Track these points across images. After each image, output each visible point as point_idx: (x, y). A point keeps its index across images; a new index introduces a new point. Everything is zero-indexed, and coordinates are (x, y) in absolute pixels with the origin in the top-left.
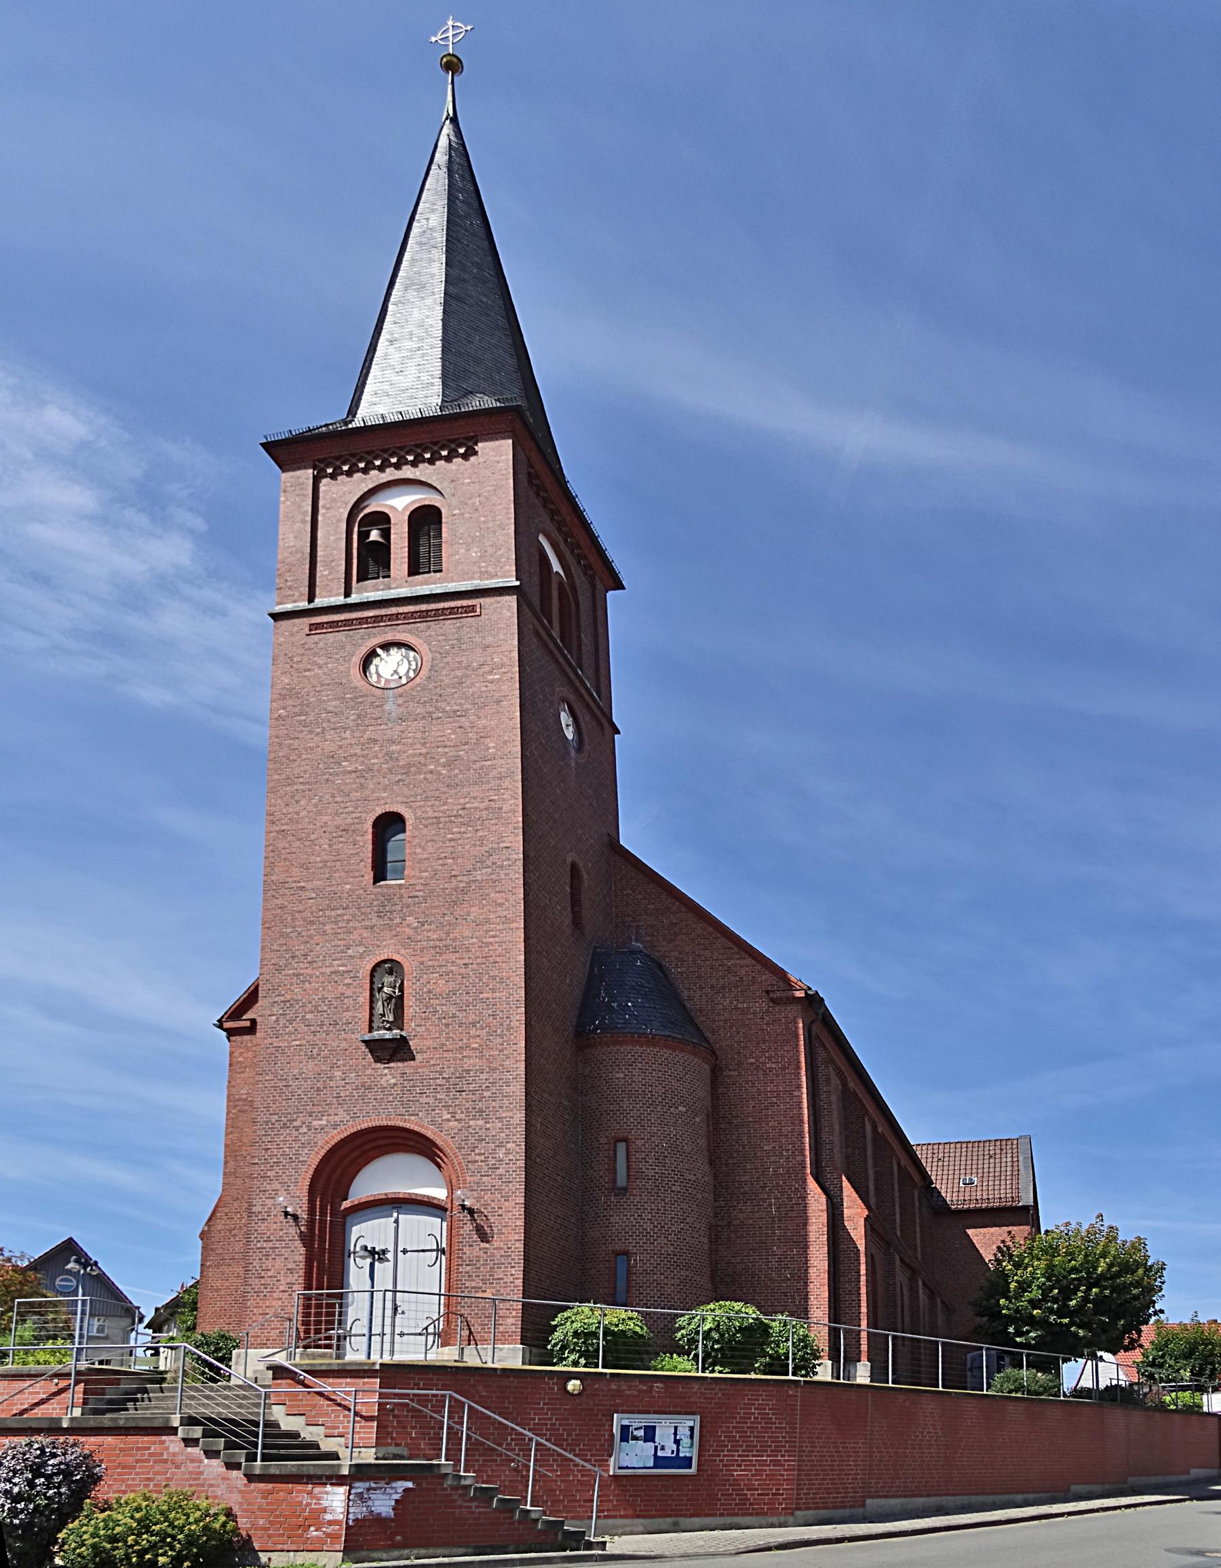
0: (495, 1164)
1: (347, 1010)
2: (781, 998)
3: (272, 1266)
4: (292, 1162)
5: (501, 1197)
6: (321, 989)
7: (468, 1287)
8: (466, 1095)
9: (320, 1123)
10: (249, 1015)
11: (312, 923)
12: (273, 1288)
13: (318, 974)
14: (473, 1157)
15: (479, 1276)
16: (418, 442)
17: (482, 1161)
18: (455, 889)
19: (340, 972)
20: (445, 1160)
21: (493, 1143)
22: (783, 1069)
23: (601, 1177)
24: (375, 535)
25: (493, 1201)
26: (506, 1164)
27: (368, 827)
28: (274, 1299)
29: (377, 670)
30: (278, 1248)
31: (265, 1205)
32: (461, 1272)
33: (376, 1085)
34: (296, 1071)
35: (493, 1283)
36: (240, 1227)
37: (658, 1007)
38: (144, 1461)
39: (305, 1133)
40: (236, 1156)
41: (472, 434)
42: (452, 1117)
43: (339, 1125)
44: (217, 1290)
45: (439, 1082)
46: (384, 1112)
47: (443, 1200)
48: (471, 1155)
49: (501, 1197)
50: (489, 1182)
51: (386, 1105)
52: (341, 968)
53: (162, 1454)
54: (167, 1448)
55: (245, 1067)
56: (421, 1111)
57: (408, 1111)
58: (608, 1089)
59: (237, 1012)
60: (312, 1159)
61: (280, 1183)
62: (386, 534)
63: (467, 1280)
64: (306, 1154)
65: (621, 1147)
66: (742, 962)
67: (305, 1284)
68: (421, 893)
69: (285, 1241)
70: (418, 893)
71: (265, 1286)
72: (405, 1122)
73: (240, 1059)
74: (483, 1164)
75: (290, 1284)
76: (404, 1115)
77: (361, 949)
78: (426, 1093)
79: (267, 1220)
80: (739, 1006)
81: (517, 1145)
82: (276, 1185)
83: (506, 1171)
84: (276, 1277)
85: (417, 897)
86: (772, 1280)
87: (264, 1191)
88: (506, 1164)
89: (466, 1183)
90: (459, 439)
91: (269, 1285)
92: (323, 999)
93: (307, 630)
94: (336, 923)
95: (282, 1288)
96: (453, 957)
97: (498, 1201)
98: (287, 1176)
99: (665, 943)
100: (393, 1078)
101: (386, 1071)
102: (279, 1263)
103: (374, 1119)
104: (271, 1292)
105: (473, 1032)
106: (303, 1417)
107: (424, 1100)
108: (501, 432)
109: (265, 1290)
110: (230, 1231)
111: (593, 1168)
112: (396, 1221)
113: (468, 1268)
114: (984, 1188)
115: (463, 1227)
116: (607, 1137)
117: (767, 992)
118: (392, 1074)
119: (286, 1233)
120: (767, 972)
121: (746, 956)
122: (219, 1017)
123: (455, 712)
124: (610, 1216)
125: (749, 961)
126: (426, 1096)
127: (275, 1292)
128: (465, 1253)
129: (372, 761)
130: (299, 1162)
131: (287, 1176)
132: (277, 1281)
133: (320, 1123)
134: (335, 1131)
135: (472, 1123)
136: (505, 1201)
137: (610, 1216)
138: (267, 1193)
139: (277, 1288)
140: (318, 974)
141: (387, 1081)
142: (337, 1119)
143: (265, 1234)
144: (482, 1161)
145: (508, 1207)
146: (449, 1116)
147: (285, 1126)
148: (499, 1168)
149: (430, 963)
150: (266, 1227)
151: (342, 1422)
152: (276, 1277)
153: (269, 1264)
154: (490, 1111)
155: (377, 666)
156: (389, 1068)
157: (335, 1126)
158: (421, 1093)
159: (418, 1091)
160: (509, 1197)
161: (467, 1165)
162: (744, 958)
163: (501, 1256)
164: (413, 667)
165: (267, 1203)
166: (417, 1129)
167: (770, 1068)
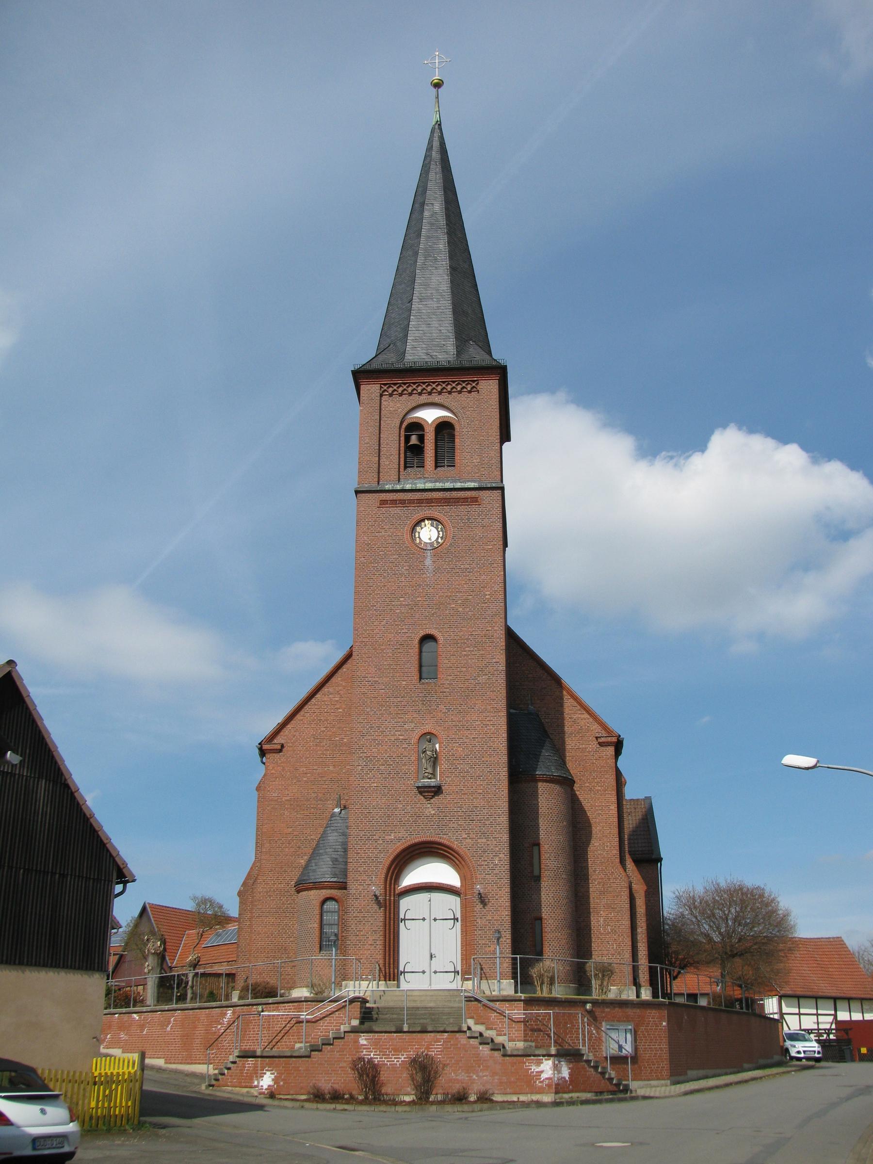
1: (405, 765)
6: (388, 750)
7: (480, 944)
9: (390, 837)
11: (382, 706)
15: (486, 937)
17: (486, 865)
18: (468, 688)
20: (463, 863)
24: (414, 440)
27: (416, 641)
29: (419, 535)
30: (366, 917)
31: (358, 889)
37: (552, 755)
38: (448, 1048)
52: (401, 737)
53: (457, 1045)
54: (460, 1041)
62: (421, 438)
66: (583, 716)
68: (448, 690)
70: (445, 690)
79: (359, 898)
81: (505, 856)
82: (364, 877)
84: (366, 935)
85: (445, 692)
86: (600, 933)
92: (390, 757)
94: (397, 706)
95: (370, 943)
96: (467, 733)
99: (539, 701)
101: (429, 806)
106: (484, 1025)
107: (451, 825)
113: (480, 932)
114: (635, 837)
117: (597, 738)
125: (586, 716)
126: (453, 823)
139: (367, 942)
144: (486, 865)
145: (501, 894)
146: (466, 836)
147: (368, 839)
149: (453, 736)
150: (359, 903)
152: (366, 935)
155: (419, 533)
156: (430, 803)
157: (399, 840)
164: (441, 535)
167: (597, 790)
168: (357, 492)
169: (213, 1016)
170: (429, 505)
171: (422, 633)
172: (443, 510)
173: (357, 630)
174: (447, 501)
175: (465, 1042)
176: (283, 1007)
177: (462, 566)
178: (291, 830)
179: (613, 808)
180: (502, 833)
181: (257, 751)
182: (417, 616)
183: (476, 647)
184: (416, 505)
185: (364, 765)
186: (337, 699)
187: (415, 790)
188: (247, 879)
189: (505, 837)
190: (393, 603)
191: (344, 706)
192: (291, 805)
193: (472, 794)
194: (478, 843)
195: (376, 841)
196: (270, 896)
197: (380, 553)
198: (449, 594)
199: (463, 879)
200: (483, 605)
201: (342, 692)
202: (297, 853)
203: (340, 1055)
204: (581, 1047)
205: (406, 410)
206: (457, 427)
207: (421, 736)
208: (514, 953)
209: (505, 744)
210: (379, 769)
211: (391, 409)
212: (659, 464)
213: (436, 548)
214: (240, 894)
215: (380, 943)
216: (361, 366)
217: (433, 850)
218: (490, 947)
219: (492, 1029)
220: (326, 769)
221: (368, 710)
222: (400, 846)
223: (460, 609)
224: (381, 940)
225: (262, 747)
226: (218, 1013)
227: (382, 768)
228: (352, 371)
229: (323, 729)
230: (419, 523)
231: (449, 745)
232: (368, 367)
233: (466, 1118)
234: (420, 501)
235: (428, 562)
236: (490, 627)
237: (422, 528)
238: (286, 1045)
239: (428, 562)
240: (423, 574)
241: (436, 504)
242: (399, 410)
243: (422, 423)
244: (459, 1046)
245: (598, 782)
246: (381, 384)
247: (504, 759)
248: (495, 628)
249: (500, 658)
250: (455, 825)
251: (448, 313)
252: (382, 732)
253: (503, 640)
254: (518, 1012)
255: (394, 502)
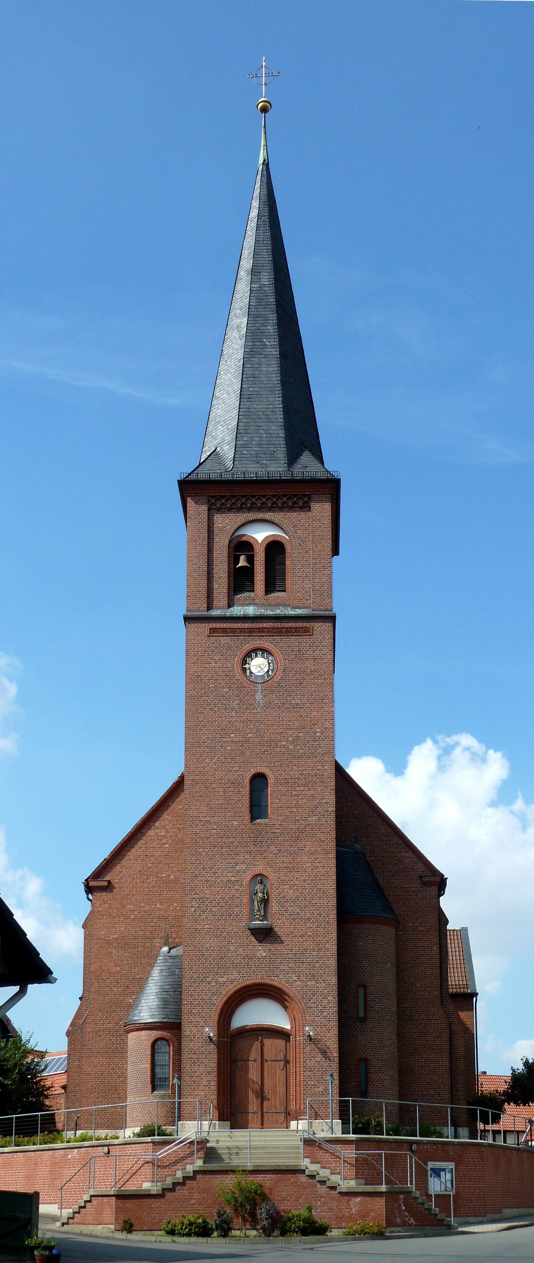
0: (322, 1009)
1: (237, 906)
2: (428, 882)
3: (198, 1070)
4: (207, 1004)
5: (326, 1030)
6: (221, 891)
7: (309, 1085)
8: (305, 965)
9: (223, 979)
10: (108, 878)
11: (214, 846)
12: (199, 1083)
13: (219, 881)
14: (309, 1005)
16: (275, 494)
17: (315, 1007)
18: (298, 829)
19: (232, 881)
21: (320, 996)
22: (428, 931)
23: (351, 1010)
24: (242, 562)
25: (322, 1032)
26: (328, 1009)
27: (247, 781)
28: (200, 1090)
30: (200, 1058)
32: (306, 1076)
33: (255, 957)
34: (207, 946)
35: (323, 1083)
36: (103, 1030)
39: (214, 986)
40: (98, 979)
41: (307, 493)
42: (298, 978)
43: (234, 981)
44: (89, 1074)
45: (290, 956)
46: (259, 974)
47: (289, 1030)
48: (309, 1003)
49: (326, 1030)
50: (319, 1021)
51: (261, 970)
52: (233, 879)
53: (297, 1183)
55: (103, 915)
56: (281, 974)
57: (274, 974)
58: (355, 952)
59: (99, 873)
60: (219, 1002)
61: (200, 1017)
62: (251, 559)
63: (309, 1081)
64: (215, 999)
65: (361, 990)
66: (407, 854)
67: (217, 1081)
69: (205, 1054)
70: (276, 831)
71: (195, 1082)
72: (272, 981)
73: (100, 909)
74: (316, 1009)
75: (209, 1081)
76: (271, 976)
77: (244, 866)
78: (283, 963)
80: (405, 886)
81: (333, 998)
82: (198, 1019)
83: (328, 1014)
84: (200, 1076)
85: (276, 833)
87: (191, 1022)
88: (328, 1009)
89: (307, 1021)
90: (299, 495)
91: (197, 1081)
92: (222, 898)
93: (207, 633)
94: (229, 847)
95: (204, 1083)
96: (297, 875)
97: (324, 1032)
98: (204, 1013)
100: (264, 952)
102: (202, 1068)
103: (254, 978)
104: (198, 1086)
105: (308, 925)
108: (325, 494)
109: (194, 1085)
110: (96, 1033)
111: (346, 1004)
112: (262, 1042)
113: (309, 1073)
115: (306, 1048)
116: (354, 984)
118: (264, 950)
119: (205, 1049)
120: (420, 862)
121: (409, 851)
122: (86, 878)
123: (297, 704)
124: (357, 1036)
126: (283, 965)
127: (200, 1086)
128: (307, 1064)
129: (249, 735)
130: (211, 1004)
131: (204, 1013)
132: (201, 1079)
133: (223, 979)
134: (232, 985)
135: (309, 983)
136: (328, 1032)
137: (357, 1036)
138: (193, 1023)
139: (202, 1083)
140: (219, 881)
141: (261, 954)
142: (233, 977)
143: (193, 1049)
144: (315, 1007)
145: (330, 1036)
146: (296, 978)
147: (202, 981)
148: (324, 1012)
149: (284, 878)
150: (194, 1045)
151: (339, 1167)
152: (200, 1076)
153: (195, 1068)
154: (319, 976)
157: (232, 982)
158: (280, 963)
159: (279, 962)
160: (330, 1030)
161: (307, 1010)
162: (408, 852)
163: (327, 1066)
165: (193, 1029)
166: (278, 985)
168: (187, 619)
169: (57, 1158)
170: (259, 634)
171: (253, 772)
172: (274, 640)
173: (189, 767)
174: (279, 632)
175: (304, 1180)
176: (130, 1148)
177: (293, 701)
178: (119, 968)
179: (436, 949)
180: (330, 976)
181: (83, 887)
182: (248, 753)
183: (306, 787)
184: (246, 634)
185: (197, 907)
186: (163, 834)
187: (248, 932)
188: (75, 1018)
189: (334, 980)
190: (224, 740)
191: (170, 842)
192: (119, 943)
193: (302, 936)
194: (307, 985)
195: (210, 982)
196: (99, 1036)
197: (211, 686)
198: (280, 731)
199: (293, 1020)
200: (314, 743)
201: (168, 827)
202: (126, 992)
203: (189, 1193)
204: (409, 1186)
205: (236, 526)
206: (288, 548)
207: (253, 877)
208: (343, 1092)
209: (334, 886)
210: (211, 911)
211: (220, 525)
212: (500, 783)
213: (268, 679)
214: (68, 1034)
215: (214, 1083)
216: (187, 474)
217: (264, 991)
218: (319, 1087)
219: (326, 1168)
220: (153, 906)
221: (201, 850)
222: (232, 988)
223: (291, 747)
224: (215, 1081)
225: (88, 883)
226: (62, 1155)
227: (214, 909)
228: (178, 480)
229: (149, 865)
230: (249, 655)
231: (280, 887)
232: (193, 477)
233: (311, 1249)
234: (251, 631)
235: (259, 696)
236: (321, 766)
237: (252, 659)
238: (133, 1184)
239: (259, 696)
240: (254, 709)
241: (267, 634)
242: (228, 527)
243: (252, 542)
244: (299, 1183)
245: (421, 923)
246: (208, 496)
247: (333, 902)
248: (326, 767)
249: (330, 799)
250: (286, 968)
251: (278, 413)
252: (215, 873)
253: (333, 780)
254: (350, 1153)
255: (224, 631)
